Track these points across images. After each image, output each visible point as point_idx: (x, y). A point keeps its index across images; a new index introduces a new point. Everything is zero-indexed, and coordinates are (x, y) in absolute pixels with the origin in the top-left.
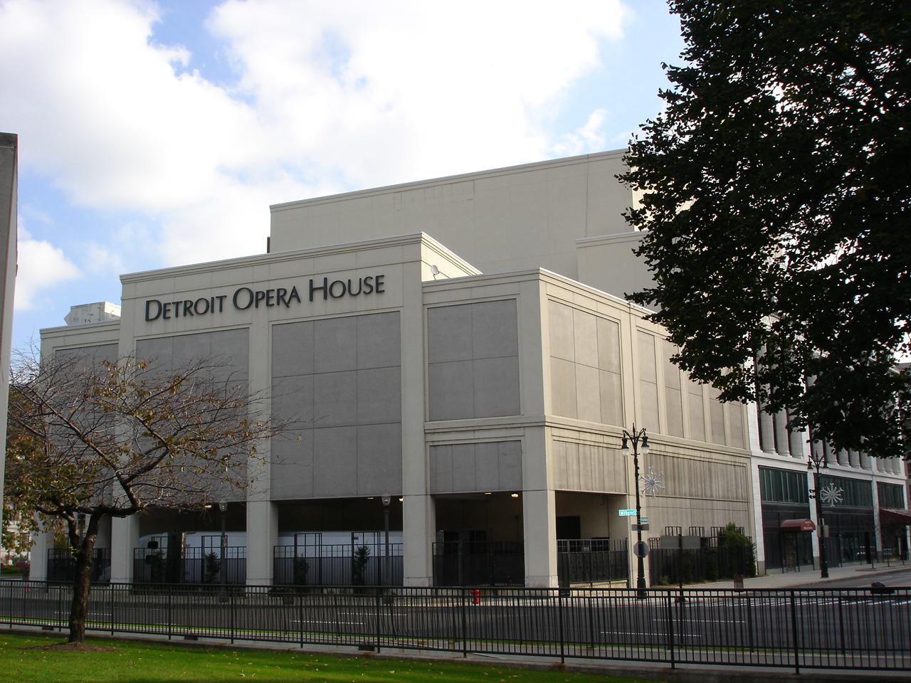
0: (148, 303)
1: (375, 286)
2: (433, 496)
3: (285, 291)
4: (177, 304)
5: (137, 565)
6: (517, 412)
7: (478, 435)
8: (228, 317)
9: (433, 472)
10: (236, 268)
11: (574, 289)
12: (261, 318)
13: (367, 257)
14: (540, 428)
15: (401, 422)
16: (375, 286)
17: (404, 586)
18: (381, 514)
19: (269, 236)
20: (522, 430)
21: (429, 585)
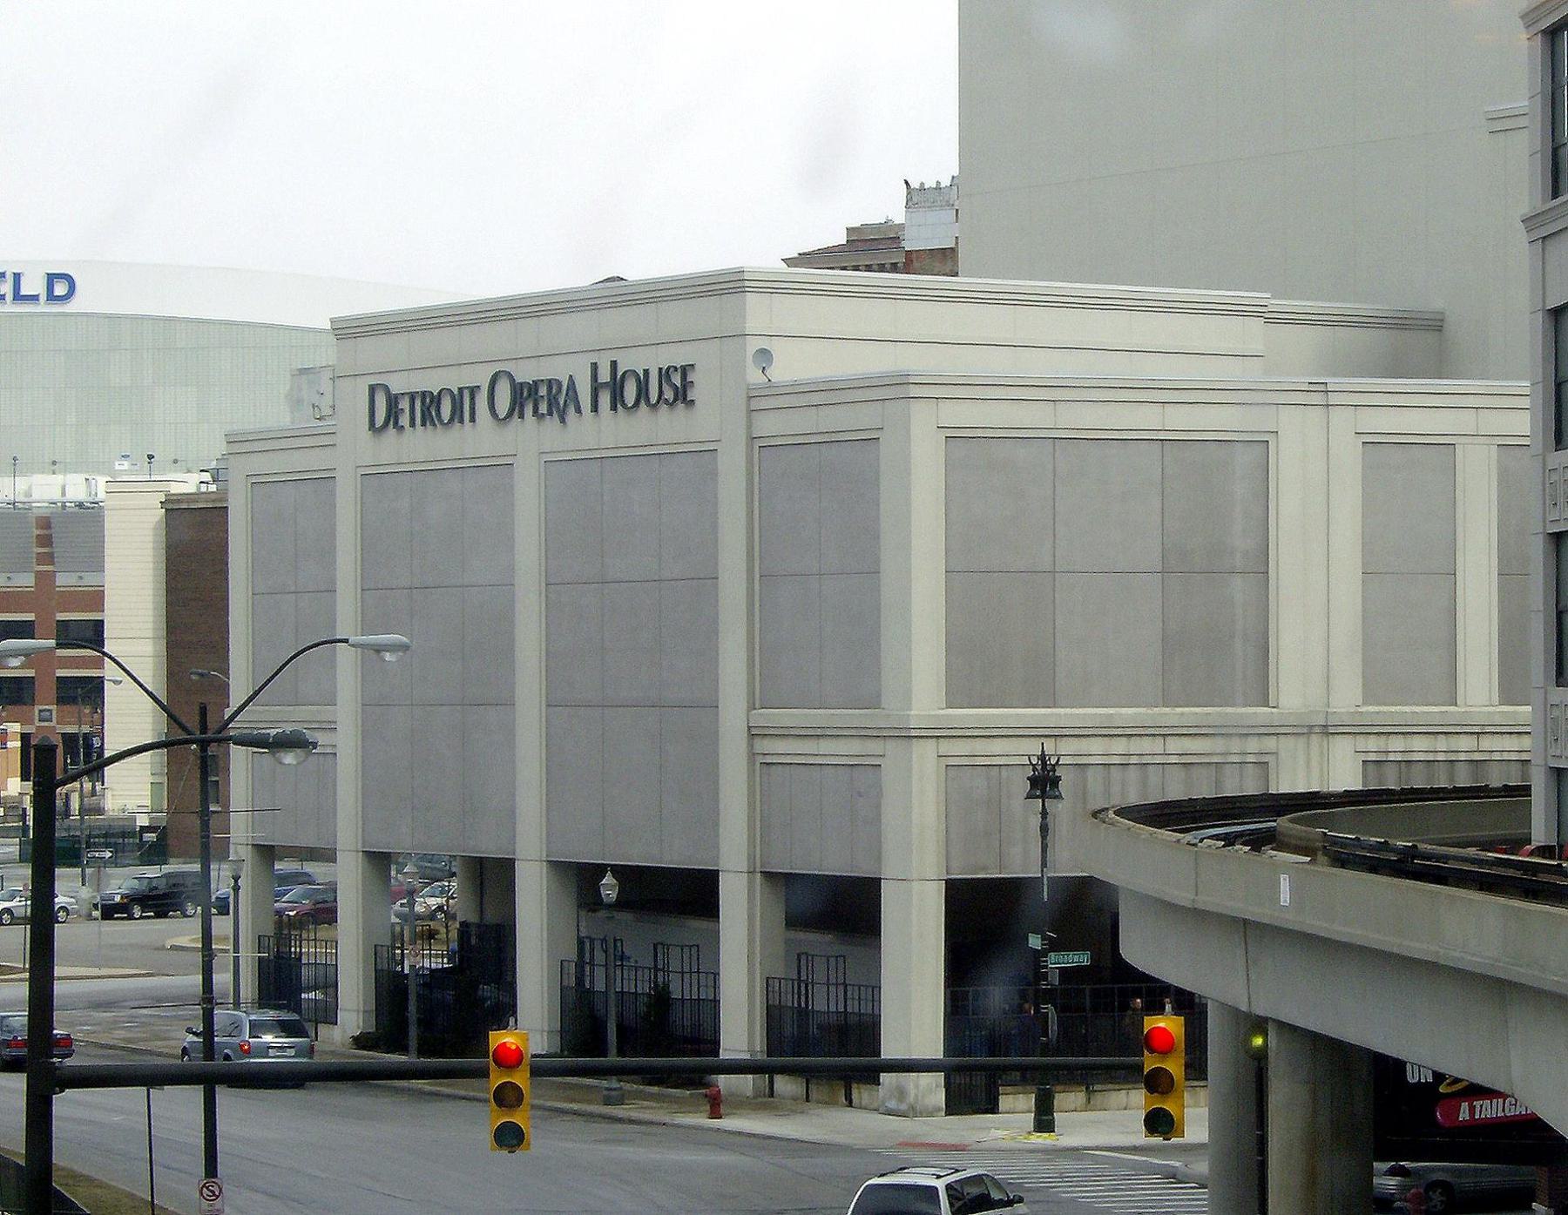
0: (372, 389)
1: (677, 388)
2: (768, 876)
3: (559, 384)
4: (412, 396)
5: (774, 1016)
6: (874, 702)
7: (826, 746)
8: (480, 438)
9: (762, 825)
10: (385, 332)
11: (1401, 400)
12: (532, 440)
13: (675, 318)
14: (904, 742)
15: (548, 705)
16: (677, 388)
17: (724, 1055)
18: (694, 894)
19: (956, 174)
20: (881, 742)
21: (752, 1051)
